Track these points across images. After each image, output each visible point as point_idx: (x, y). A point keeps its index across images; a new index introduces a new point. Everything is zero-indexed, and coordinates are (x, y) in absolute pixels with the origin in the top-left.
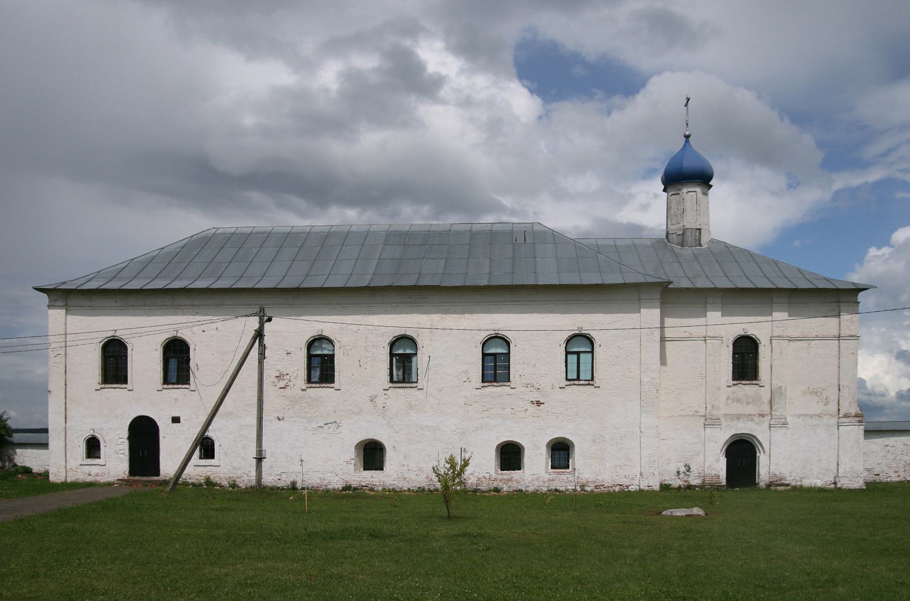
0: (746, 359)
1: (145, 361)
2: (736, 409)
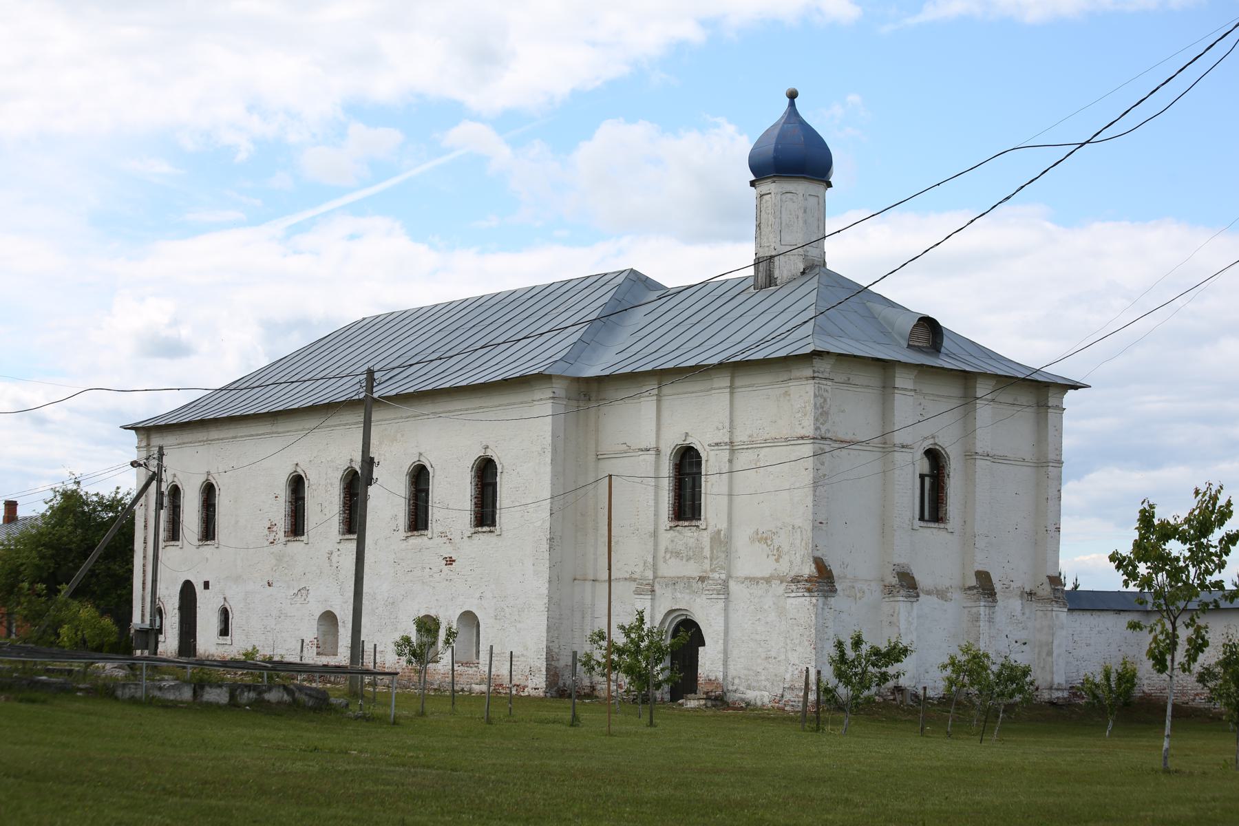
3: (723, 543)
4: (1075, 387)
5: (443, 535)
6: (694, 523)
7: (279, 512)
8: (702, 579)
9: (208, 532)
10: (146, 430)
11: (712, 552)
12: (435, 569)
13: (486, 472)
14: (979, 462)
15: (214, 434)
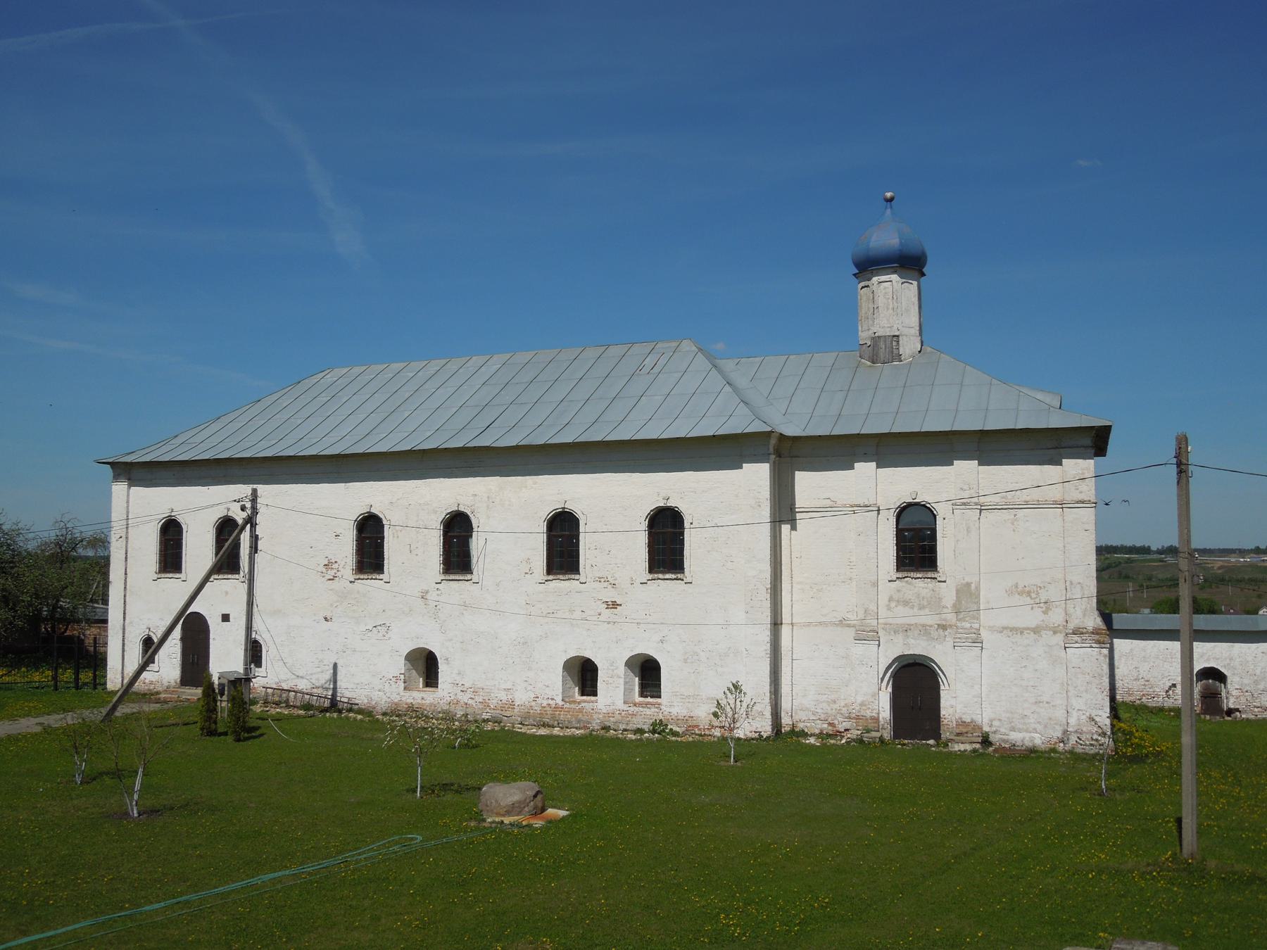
0: (916, 546)
1: (199, 549)
2: (902, 615)
3: (967, 593)
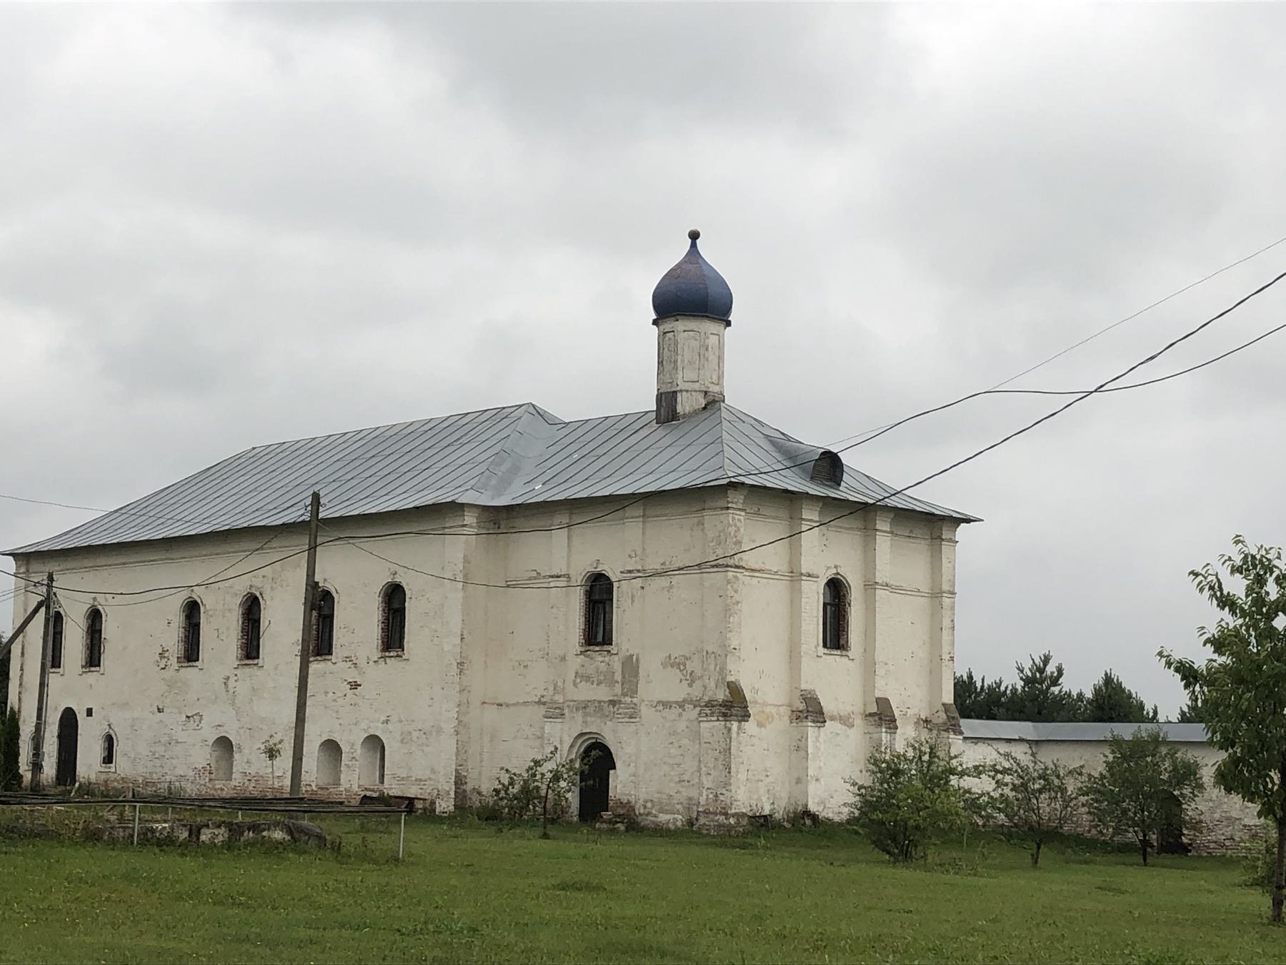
2: (587, 692)
3: (631, 667)
4: (968, 521)
5: (347, 659)
6: (606, 648)
7: (173, 638)
8: (613, 703)
9: (93, 658)
10: (25, 558)
11: (624, 677)
12: (339, 694)
13: (394, 598)
14: (878, 592)
15: (101, 561)
